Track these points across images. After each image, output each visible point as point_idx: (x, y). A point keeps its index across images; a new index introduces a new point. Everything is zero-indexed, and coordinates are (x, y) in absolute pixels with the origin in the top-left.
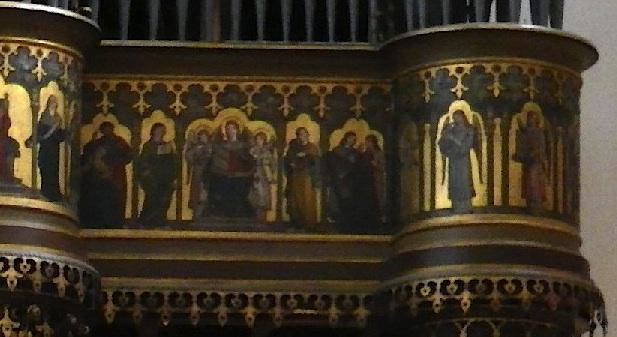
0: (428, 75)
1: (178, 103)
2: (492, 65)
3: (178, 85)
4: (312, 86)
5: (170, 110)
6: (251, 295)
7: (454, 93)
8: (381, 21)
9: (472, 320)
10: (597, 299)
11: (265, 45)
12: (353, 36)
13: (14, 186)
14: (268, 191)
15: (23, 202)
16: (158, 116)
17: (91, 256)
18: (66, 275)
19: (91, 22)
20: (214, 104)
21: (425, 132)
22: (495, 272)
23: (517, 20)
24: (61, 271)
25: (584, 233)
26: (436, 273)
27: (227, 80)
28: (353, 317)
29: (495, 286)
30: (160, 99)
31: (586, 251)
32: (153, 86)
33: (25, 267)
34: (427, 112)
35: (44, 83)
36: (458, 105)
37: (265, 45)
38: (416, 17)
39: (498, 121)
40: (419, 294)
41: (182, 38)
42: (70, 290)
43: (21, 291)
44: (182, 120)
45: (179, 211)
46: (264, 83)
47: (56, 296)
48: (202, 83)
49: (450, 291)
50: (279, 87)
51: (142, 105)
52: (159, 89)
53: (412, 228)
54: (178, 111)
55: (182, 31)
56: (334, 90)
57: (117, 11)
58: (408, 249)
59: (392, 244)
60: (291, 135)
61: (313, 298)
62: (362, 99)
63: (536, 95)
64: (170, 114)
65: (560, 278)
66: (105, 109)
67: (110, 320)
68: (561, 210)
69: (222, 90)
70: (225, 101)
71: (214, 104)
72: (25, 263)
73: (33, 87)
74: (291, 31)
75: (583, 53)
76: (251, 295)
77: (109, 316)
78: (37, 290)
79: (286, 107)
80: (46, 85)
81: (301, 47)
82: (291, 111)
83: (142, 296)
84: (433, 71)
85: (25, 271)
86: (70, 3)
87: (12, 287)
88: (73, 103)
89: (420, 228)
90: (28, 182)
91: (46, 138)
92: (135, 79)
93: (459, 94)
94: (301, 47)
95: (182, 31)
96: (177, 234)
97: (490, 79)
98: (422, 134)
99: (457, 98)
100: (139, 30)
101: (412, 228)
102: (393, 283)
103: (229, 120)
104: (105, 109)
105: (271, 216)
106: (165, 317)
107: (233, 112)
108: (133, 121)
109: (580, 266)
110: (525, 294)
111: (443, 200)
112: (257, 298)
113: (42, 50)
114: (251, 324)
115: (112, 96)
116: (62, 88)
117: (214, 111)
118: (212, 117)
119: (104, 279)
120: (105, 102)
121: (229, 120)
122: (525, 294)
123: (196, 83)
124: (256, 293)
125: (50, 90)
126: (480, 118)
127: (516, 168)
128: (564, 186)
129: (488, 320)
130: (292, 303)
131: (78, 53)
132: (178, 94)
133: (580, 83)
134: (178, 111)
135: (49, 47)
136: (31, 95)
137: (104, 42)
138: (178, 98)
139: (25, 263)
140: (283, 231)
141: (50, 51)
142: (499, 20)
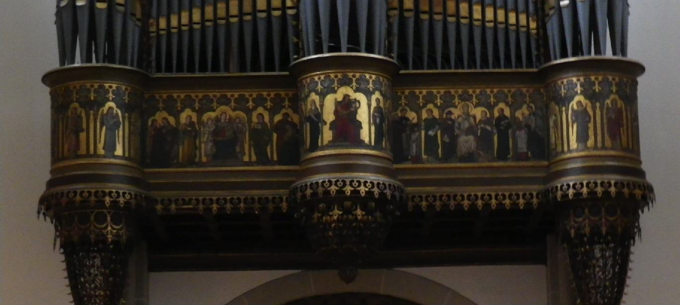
0: (562, 83)
3: (438, 91)
4: (227, 94)
5: (252, 108)
6: (214, 198)
8: (538, 57)
9: (97, 211)
12: (163, 70)
13: (360, 144)
15: (364, 151)
16: (260, 110)
17: (400, 177)
18: (390, 189)
20: (215, 104)
21: (562, 111)
23: (605, 54)
24: (387, 186)
25: (644, 156)
26: (571, 180)
27: (203, 92)
28: (224, 209)
29: (93, 194)
30: (188, 103)
31: (644, 166)
36: (577, 98)
37: (491, 70)
39: (598, 104)
42: (393, 196)
45: (200, 157)
46: (186, 94)
47: (582, 198)
48: (245, 93)
49: (113, 196)
50: (247, 95)
51: (251, 104)
52: (430, 94)
53: (559, 158)
54: (269, 107)
55: (277, 66)
56: (444, 92)
58: (563, 168)
59: (548, 167)
61: (190, 200)
63: (616, 91)
64: (265, 108)
65: (396, 184)
66: (287, 106)
67: (522, 208)
68: (631, 147)
70: (220, 103)
71: (215, 104)
72: (355, 182)
73: (368, 94)
74: (493, 63)
75: (637, 69)
76: (214, 198)
78: (321, 196)
79: (251, 104)
80: (374, 94)
82: (424, 104)
83: (245, 199)
84: (565, 81)
85: (370, 187)
88: (388, 102)
89: (555, 161)
90: (367, 140)
94: (486, 70)
95: (277, 66)
97: (594, 84)
98: (561, 112)
99: (110, 101)
100: (418, 64)
101: (559, 158)
102: (549, 186)
103: (226, 111)
104: (287, 106)
105: (246, 159)
106: (257, 210)
108: (176, 115)
109: (641, 174)
110: (78, 198)
111: (574, 144)
112: (218, 200)
113: (371, 77)
114: (424, 210)
115: (164, 101)
116: (382, 94)
117: (215, 107)
118: (214, 111)
119: (406, 189)
120: (161, 105)
121: (226, 111)
122: (78, 198)
123: (242, 93)
124: (204, 197)
125: (377, 95)
126: (623, 106)
128: (59, 144)
129: (105, 211)
131: (388, 77)
133: (637, 83)
134: (269, 107)
135: (322, 74)
136: (367, 98)
137: (402, 72)
138: (233, 101)
139: (327, 183)
140: (252, 166)
141: (324, 75)
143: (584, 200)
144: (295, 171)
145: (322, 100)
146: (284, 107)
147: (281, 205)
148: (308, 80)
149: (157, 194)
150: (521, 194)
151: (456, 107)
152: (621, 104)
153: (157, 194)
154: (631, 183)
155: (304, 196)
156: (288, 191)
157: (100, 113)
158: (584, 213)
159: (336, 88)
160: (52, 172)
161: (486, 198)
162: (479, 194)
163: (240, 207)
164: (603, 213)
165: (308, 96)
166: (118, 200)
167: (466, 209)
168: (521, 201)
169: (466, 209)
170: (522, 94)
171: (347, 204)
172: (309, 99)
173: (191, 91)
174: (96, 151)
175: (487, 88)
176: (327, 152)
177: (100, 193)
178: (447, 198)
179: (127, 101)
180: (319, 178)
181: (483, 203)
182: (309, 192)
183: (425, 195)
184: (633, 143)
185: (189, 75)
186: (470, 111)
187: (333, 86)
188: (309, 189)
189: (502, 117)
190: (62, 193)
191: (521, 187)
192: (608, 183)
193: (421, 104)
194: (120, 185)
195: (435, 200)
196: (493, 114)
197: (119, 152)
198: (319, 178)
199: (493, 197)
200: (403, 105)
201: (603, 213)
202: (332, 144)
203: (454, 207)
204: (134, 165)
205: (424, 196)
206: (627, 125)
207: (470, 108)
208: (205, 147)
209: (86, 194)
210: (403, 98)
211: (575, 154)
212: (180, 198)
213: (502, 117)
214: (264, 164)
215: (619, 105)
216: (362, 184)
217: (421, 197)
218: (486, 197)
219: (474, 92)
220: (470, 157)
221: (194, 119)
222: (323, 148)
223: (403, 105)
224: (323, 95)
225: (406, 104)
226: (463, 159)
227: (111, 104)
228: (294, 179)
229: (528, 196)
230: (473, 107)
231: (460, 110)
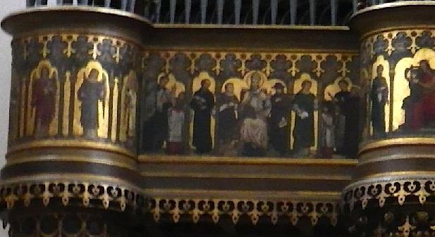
1: (218, 67)
2: (421, 31)
4: (312, 55)
7: (410, 50)
12: (313, 22)
32: (302, 57)
33: (76, 189)
39: (68, 74)
41: (333, 24)
43: (410, 203)
44: (220, 78)
51: (294, 71)
52: (306, 59)
57: (233, 7)
60: (197, 86)
62: (246, 62)
69: (324, 59)
77: (176, 217)
86: (129, 3)
92: (239, 51)
93: (95, 56)
127: (78, 104)
130: (374, 191)
131: (134, 40)
132: (294, 62)
134: (218, 72)
139: (412, 185)
143: (84, 208)
144: (353, 166)
145: (393, 65)
146: (340, 74)
147: (250, 213)
148: (375, 37)
149: (157, 193)
150: (177, 201)
151: (242, 78)
152: (103, 75)
153: (157, 193)
154: (21, 186)
155: (359, 204)
156: (340, 194)
157: (32, 76)
158: (79, 227)
159: (413, 51)
160: (7, 157)
161: (226, 207)
162: (236, 201)
163: (312, 217)
164: (60, 228)
165: (375, 60)
166: (101, 198)
167: (255, 222)
168: (176, 211)
169: (255, 222)
170: (176, 59)
171: (423, 215)
172: (376, 65)
173: (235, 49)
174: (72, 130)
175: (236, 51)
176: (400, 141)
177: (38, 187)
178: (268, 207)
179: (117, 60)
180: (390, 177)
181: (241, 213)
182: (366, 198)
183: (317, 202)
184: (19, 124)
185: (178, 25)
186: (261, 84)
187: (409, 48)
188: (383, 192)
189: (204, 92)
190: (363, 188)
191: (177, 191)
192: (79, 185)
193: (193, 72)
194: (104, 178)
195: (291, 209)
196: (292, 90)
197: (102, 131)
198: (390, 177)
199: (216, 205)
200: (344, 74)
201: (60, 228)
202: (405, 130)
203: (336, 223)
204: (124, 151)
205: (315, 203)
206: (26, 104)
207: (261, 81)
208: (254, 128)
209: (76, 189)
210: (344, 65)
211: (100, 145)
212: (285, 202)
213: (204, 92)
214: (283, 154)
215: (100, 78)
216: (402, 187)
217: (310, 205)
218: (226, 206)
219: (243, 57)
220: (250, 149)
221: (212, 88)
222: (394, 134)
223: (344, 74)
224: (394, 59)
225: (347, 74)
226: (169, 151)
227: (96, 65)
228: (349, 178)
229: (167, 204)
230: (266, 78)
231: (247, 82)
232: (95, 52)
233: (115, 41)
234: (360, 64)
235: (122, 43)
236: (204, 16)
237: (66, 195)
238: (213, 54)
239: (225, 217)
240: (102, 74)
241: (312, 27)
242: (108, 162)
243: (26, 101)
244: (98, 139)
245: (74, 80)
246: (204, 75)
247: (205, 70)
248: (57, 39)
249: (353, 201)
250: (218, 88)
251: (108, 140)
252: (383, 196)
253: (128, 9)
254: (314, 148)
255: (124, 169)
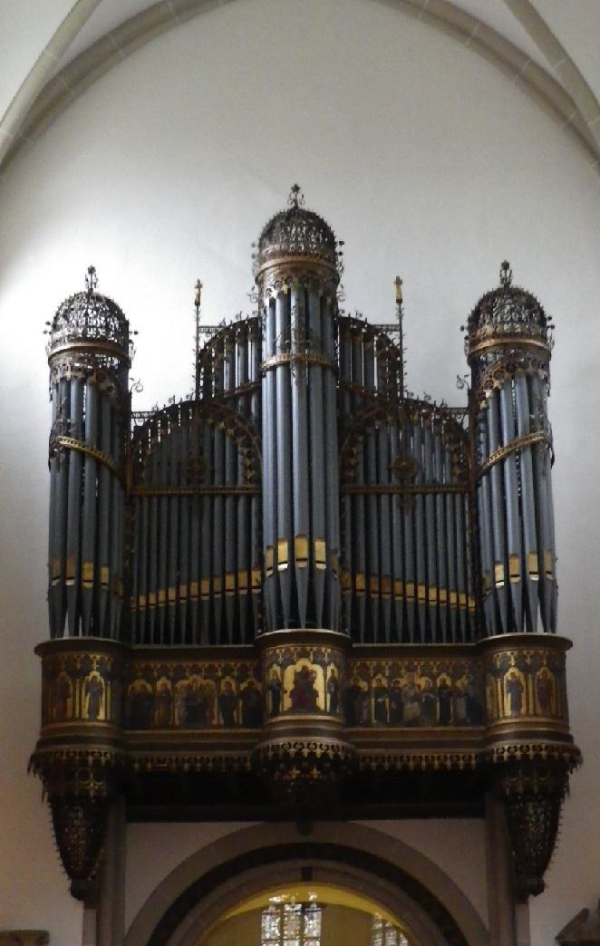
3: (387, 664)
8: (476, 632)
10: (578, 752)
11: (165, 647)
13: (316, 710)
14: (412, 709)
19: (348, 636)
22: (531, 742)
31: (572, 732)
34: (499, 673)
35: (329, 664)
38: (491, 631)
40: (497, 752)
44: (174, 681)
51: (220, 674)
60: (438, 683)
73: (324, 666)
74: (426, 636)
75: (567, 644)
79: (220, 674)
81: (430, 645)
87: (319, 756)
91: (333, 685)
94: (430, 645)
95: (388, 639)
96: (216, 731)
97: (525, 657)
105: (215, 722)
107: (195, 676)
108: (153, 682)
109: (570, 738)
111: (508, 712)
113: (326, 650)
116: (336, 665)
121: (199, 680)
125: (332, 666)
133: (565, 657)
142: (528, 631)
149: (135, 754)
171: (305, 764)
180: (281, 741)
182: (271, 753)
189: (444, 686)
195: (384, 761)
197: (102, 716)
198: (281, 741)
202: (292, 711)
208: (179, 712)
213: (444, 686)
224: (284, 667)
227: (95, 673)
232: (95, 666)
233: (107, 658)
234: (260, 672)
235: (112, 659)
236: (423, 637)
237: (531, 753)
238: (447, 662)
239: (455, 765)
240: (100, 679)
241: (375, 645)
242: (104, 735)
243: (527, 694)
244: (505, 718)
245: (502, 681)
246: (444, 676)
247: (445, 672)
248: (87, 657)
249: (262, 756)
250: (173, 687)
251: (528, 714)
252: (281, 752)
253: (334, 630)
254: (451, 721)
255: (515, 732)
